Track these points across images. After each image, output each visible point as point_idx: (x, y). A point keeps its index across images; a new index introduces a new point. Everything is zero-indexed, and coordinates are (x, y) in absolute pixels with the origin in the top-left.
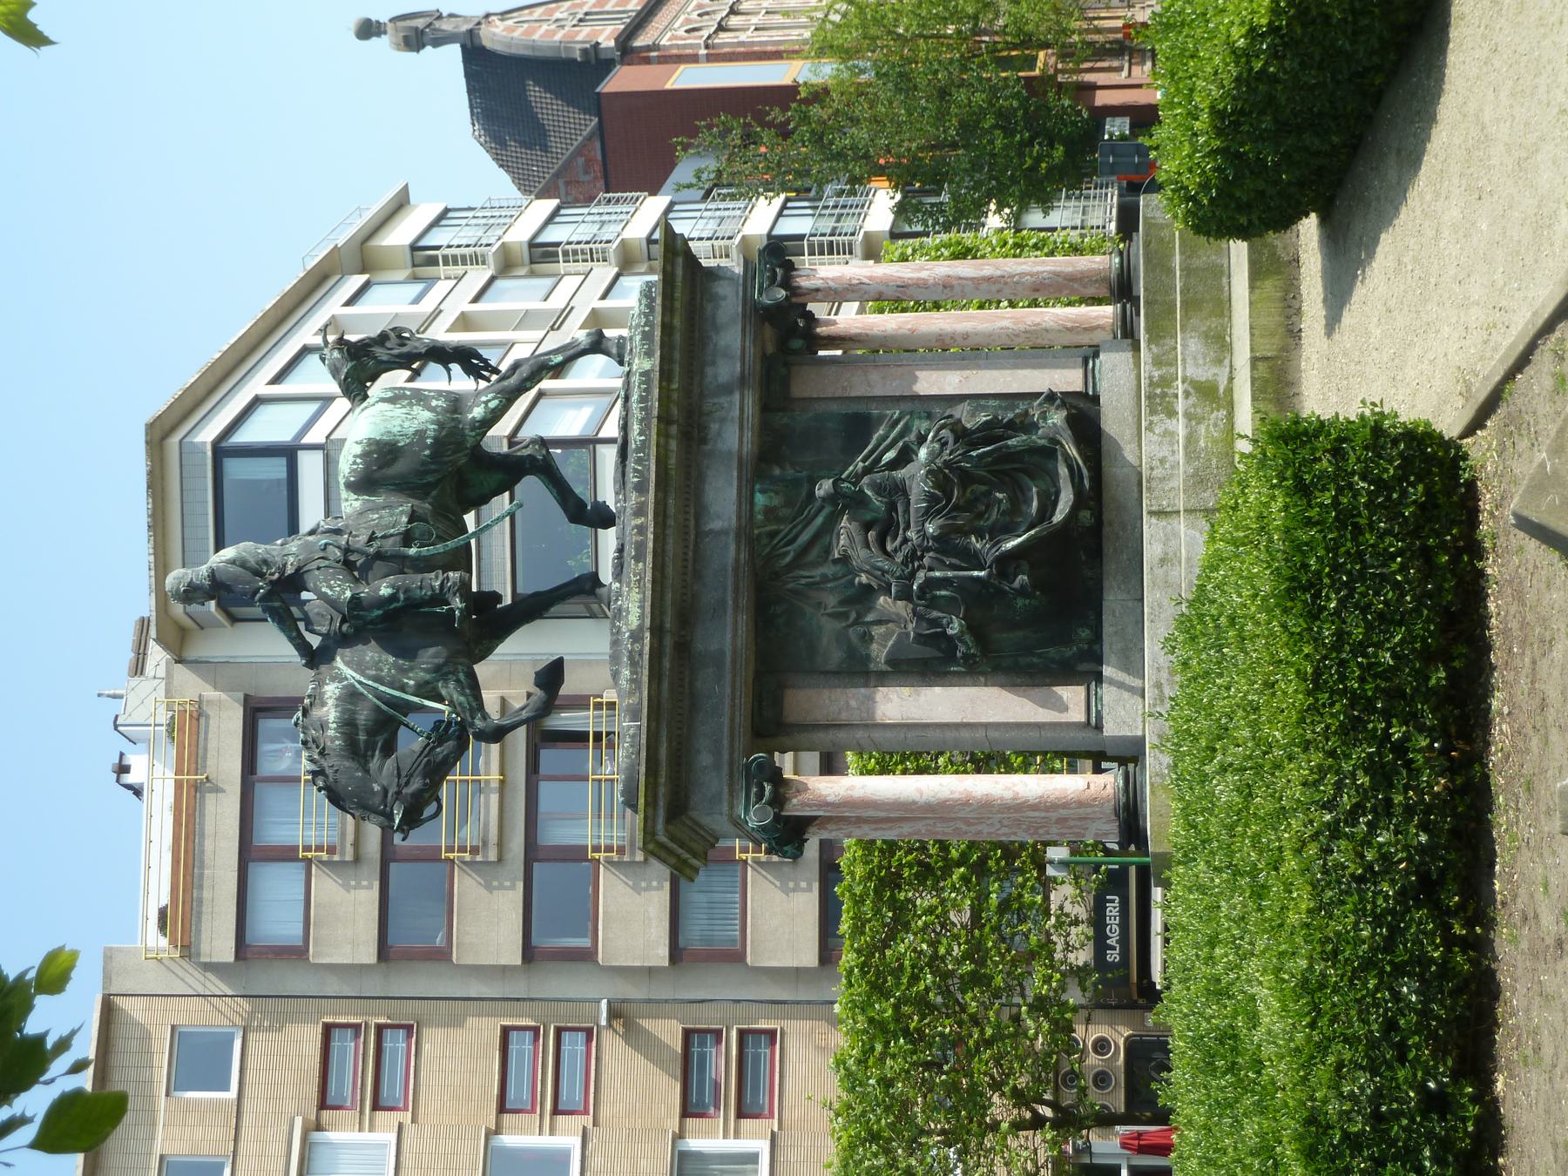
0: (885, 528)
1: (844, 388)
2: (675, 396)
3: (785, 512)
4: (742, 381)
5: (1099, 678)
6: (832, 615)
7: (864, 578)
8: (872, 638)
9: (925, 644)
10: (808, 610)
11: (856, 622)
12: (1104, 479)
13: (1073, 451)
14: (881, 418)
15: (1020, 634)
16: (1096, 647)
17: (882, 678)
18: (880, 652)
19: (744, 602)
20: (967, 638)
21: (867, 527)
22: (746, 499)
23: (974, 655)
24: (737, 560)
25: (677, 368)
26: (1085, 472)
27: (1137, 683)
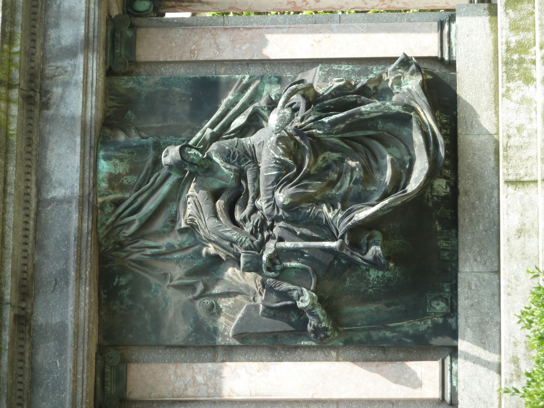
0: (233, 197)
1: (192, 52)
2: (17, 59)
3: (131, 180)
4: (87, 43)
5: (454, 352)
6: (176, 287)
7: (211, 249)
8: (219, 311)
9: (274, 317)
10: (153, 281)
11: (203, 294)
12: (460, 148)
13: (428, 118)
14: (230, 83)
15: (372, 307)
16: (450, 321)
17: (230, 352)
18: (227, 326)
19: (87, 272)
20: (319, 311)
21: (215, 195)
22: (89, 167)
23: (326, 329)
24: (80, 229)
25: (19, 31)
26: (440, 139)
27: (492, 357)
